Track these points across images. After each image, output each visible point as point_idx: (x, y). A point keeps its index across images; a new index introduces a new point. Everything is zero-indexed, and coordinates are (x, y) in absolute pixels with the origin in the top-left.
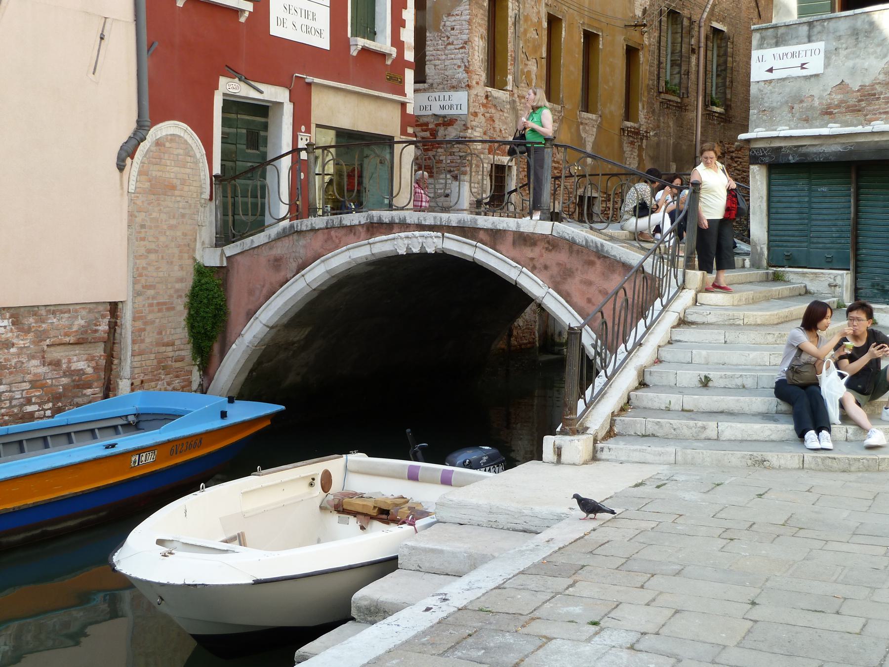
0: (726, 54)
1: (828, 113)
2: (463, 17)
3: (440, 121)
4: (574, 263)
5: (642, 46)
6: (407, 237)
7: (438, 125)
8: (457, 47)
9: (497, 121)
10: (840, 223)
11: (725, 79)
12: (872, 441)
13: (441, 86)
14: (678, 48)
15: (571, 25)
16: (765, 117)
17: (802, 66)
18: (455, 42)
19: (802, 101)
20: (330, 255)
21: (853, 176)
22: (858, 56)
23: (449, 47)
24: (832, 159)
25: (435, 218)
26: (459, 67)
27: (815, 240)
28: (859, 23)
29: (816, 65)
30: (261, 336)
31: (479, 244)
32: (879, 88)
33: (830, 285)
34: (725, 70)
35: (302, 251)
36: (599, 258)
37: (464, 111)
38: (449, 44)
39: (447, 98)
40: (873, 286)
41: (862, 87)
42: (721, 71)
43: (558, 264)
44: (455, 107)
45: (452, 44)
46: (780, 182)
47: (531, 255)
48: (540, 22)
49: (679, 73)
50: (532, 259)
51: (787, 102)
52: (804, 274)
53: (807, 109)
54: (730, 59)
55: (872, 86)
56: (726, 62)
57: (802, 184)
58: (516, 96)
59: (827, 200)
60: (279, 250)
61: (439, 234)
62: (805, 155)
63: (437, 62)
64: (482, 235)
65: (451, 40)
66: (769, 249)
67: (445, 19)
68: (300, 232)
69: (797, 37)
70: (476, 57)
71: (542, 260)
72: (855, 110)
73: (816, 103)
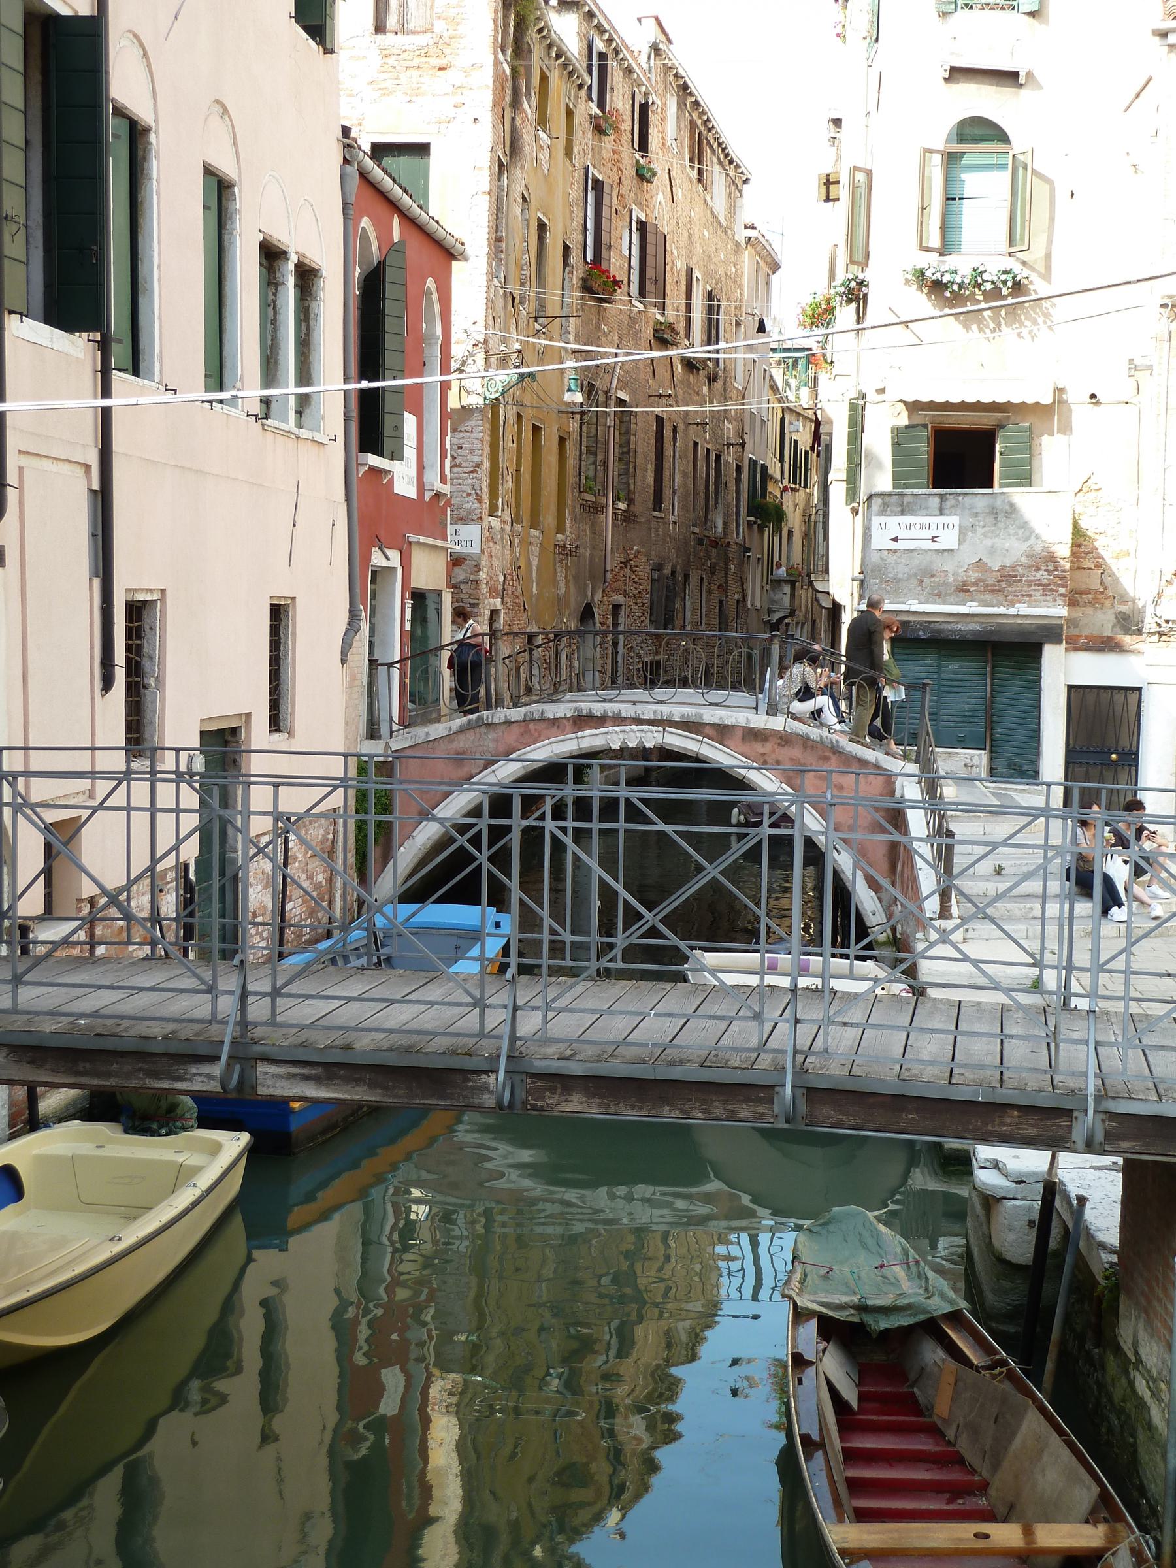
0: (628, 432)
1: (963, 590)
2: (475, 435)
4: (810, 759)
6: (624, 732)
8: (467, 470)
10: (973, 701)
11: (628, 463)
12: (1154, 914)
14: (593, 430)
16: (888, 588)
17: (933, 539)
19: (933, 576)
21: (990, 655)
22: (998, 536)
24: (970, 637)
25: (655, 712)
26: (469, 494)
27: (945, 718)
28: (998, 503)
29: (949, 539)
30: (436, 837)
32: (1020, 570)
33: (966, 765)
34: (628, 452)
35: (492, 745)
36: (834, 753)
37: (477, 549)
40: (1009, 765)
41: (1003, 567)
42: (623, 453)
45: (460, 466)
47: (762, 750)
49: (594, 463)
50: (763, 754)
51: (915, 575)
53: (939, 584)
54: (633, 438)
55: (1014, 567)
56: (629, 442)
57: (930, 659)
59: (959, 677)
60: (462, 743)
61: (661, 729)
62: (939, 631)
68: (489, 725)
69: (927, 508)
71: (773, 756)
72: (995, 590)
73: (950, 579)
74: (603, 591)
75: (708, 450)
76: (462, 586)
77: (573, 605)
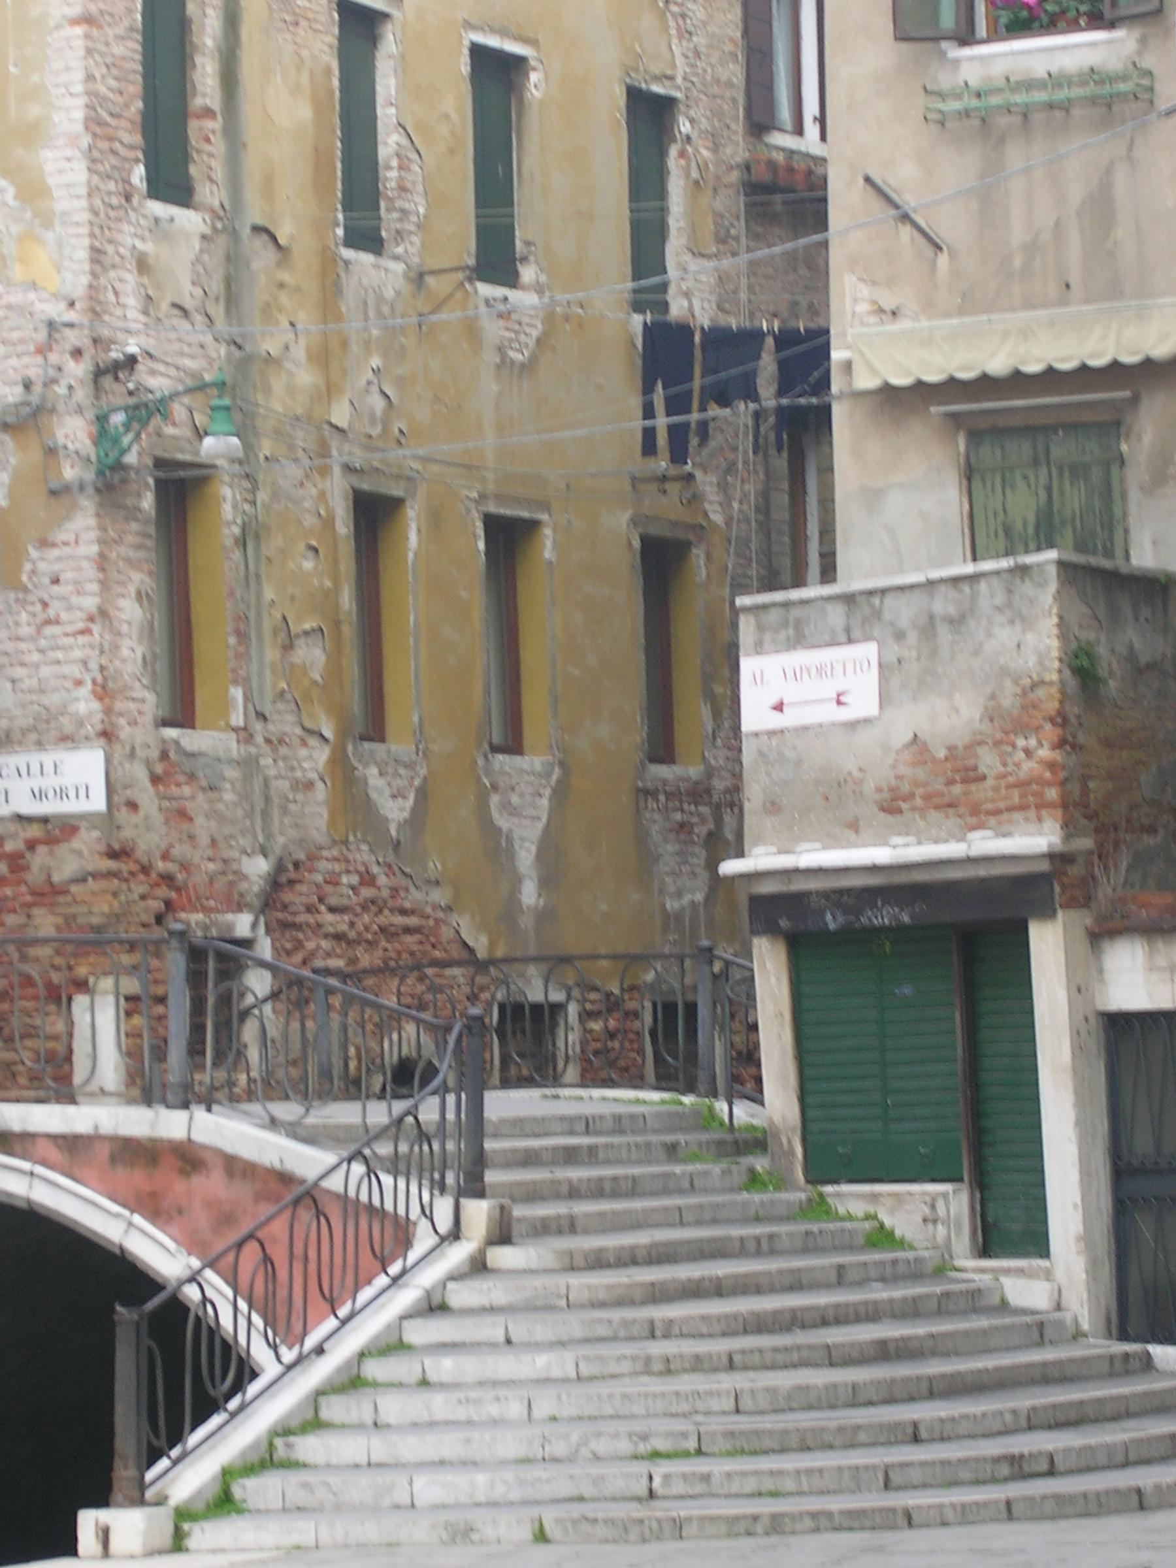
3: (35, 831)
5: (701, 530)
7: (31, 845)
8: (70, 629)
9: (200, 821)
13: (33, 736)
15: (435, 521)
18: (64, 616)
23: (49, 630)
26: (79, 683)
31: (40, 1170)
37: (97, 803)
38: (48, 622)
39: (49, 768)
44: (72, 794)
45: (56, 622)
48: (328, 522)
52: (874, 1197)
58: (260, 739)
63: (19, 672)
65: (51, 613)
66: (804, 1140)
67: (33, 553)
70: (125, 652)
76: (74, 889)
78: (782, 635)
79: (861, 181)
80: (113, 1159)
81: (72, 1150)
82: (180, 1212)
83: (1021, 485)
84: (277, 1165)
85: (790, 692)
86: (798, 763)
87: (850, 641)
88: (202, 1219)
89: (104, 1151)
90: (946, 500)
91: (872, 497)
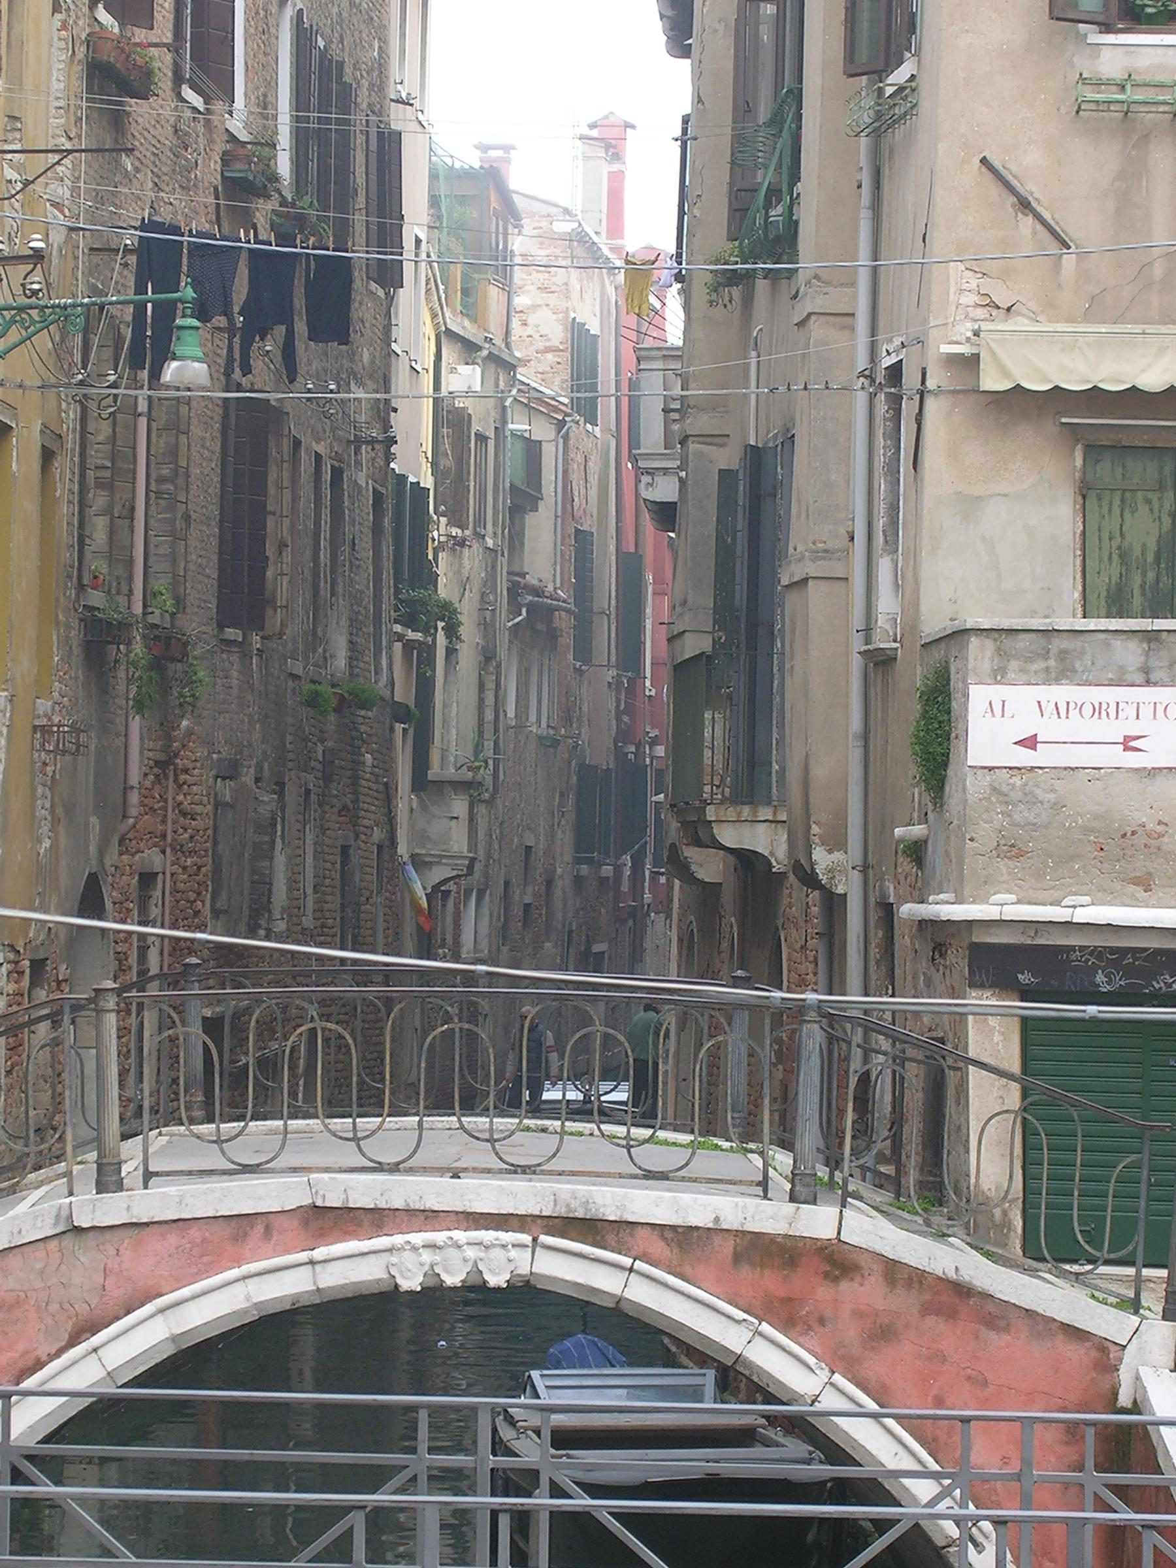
4: (904, 1302)
6: (432, 1246)
17: (1127, 744)
20: (186, 1292)
43: (857, 1314)
46: (484, 930)
61: (526, 1238)
64: (644, 1239)
74: (122, 841)
75: (318, 457)
77: (64, 881)
78: (1040, 665)
79: (976, 161)
80: (737, 1257)
81: (683, 1245)
82: (822, 1321)
83: (1143, 509)
84: (951, 1274)
85: (1046, 729)
86: (1058, 806)
87: (1148, 683)
88: (851, 1333)
89: (728, 1247)
90: (1060, 517)
91: (969, 506)
